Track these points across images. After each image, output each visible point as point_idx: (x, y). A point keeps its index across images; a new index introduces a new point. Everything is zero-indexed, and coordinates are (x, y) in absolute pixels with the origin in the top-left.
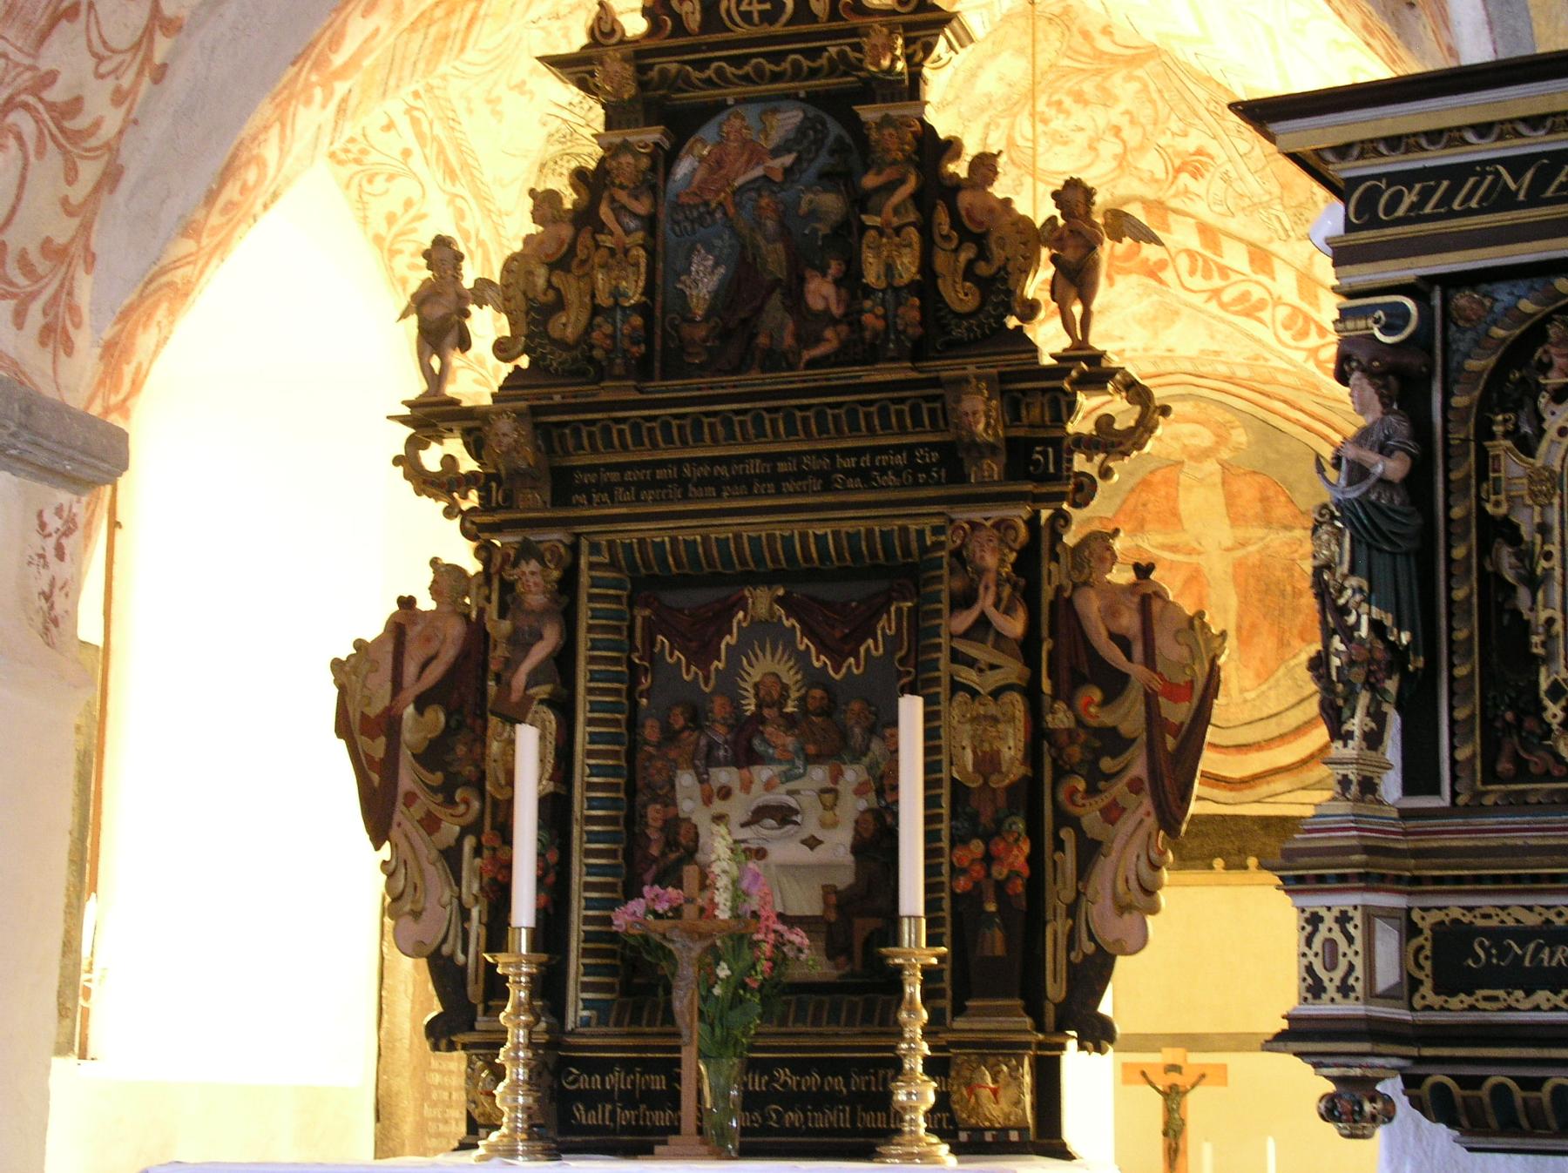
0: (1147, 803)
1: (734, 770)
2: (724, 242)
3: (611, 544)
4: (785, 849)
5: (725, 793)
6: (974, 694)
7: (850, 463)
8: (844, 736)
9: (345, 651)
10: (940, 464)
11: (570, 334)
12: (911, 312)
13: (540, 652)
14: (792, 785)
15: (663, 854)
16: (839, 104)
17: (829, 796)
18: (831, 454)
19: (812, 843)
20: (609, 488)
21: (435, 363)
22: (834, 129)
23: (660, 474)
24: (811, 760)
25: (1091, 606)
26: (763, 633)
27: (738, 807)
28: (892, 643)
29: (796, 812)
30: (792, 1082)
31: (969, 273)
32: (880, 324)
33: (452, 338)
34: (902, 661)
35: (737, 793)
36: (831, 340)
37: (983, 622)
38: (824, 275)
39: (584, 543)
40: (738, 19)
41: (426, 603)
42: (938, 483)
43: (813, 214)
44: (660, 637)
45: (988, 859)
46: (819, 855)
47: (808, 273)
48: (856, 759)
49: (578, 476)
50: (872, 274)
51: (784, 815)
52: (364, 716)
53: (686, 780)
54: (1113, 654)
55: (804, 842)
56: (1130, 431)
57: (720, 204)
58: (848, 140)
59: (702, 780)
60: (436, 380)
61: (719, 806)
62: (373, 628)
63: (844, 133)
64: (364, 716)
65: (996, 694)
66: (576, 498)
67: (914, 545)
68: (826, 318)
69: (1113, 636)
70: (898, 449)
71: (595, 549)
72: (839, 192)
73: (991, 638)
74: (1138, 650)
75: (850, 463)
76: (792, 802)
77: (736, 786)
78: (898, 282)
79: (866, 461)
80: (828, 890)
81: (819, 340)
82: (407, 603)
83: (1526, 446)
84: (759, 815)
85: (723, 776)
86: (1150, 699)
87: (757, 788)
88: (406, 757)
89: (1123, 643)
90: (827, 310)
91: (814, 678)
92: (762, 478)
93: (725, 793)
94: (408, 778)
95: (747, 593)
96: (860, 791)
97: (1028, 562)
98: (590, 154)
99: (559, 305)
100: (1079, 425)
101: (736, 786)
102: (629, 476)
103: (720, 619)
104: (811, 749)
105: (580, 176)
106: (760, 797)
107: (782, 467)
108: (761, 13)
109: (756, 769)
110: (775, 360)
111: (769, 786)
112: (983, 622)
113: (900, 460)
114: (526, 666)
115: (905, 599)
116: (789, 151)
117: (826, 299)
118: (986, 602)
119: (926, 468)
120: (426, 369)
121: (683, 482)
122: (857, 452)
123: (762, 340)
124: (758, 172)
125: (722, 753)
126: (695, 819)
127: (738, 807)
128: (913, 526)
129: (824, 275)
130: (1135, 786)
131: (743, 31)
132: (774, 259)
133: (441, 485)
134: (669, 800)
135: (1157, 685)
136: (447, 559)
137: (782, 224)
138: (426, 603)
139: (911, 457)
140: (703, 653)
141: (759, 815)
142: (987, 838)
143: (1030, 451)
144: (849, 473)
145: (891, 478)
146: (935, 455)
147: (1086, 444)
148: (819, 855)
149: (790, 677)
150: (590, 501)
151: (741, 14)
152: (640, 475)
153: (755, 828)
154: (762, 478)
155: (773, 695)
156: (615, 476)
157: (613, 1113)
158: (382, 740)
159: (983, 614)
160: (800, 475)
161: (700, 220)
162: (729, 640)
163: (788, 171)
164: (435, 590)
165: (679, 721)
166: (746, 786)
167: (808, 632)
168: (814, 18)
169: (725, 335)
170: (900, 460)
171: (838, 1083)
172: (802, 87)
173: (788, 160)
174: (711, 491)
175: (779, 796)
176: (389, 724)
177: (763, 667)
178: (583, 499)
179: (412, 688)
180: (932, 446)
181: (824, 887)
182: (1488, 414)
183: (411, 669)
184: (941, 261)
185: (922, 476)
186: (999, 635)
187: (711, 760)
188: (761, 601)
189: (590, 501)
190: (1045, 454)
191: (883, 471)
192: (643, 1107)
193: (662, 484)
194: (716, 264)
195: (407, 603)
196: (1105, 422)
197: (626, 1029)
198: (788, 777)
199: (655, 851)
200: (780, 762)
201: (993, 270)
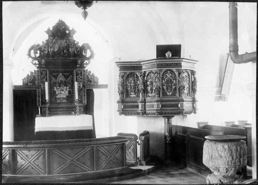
4: (63, 92)
9: (23, 78)
11: (46, 53)
17: (66, 89)
19: (65, 92)
24: (65, 86)
36: (66, 55)
37: (79, 77)
41: (30, 75)
51: (63, 90)
53: (55, 88)
54: (91, 80)
56: (88, 63)
59: (56, 88)
61: (58, 90)
62: (25, 77)
69: (91, 78)
79: (70, 64)
80: (66, 96)
82: (28, 75)
83: (128, 81)
93: (58, 89)
96: (68, 88)
98: (47, 39)
100: (85, 63)
101: (59, 88)
103: (57, 75)
106: (61, 89)
111: (62, 88)
112: (79, 77)
118: (79, 76)
127: (59, 90)
133: (35, 64)
134: (54, 89)
136: (32, 71)
138: (30, 75)
147: (85, 64)
148: (66, 93)
164: (31, 73)
175: (62, 89)
182: (35, 134)
195: (28, 75)
196: (86, 62)
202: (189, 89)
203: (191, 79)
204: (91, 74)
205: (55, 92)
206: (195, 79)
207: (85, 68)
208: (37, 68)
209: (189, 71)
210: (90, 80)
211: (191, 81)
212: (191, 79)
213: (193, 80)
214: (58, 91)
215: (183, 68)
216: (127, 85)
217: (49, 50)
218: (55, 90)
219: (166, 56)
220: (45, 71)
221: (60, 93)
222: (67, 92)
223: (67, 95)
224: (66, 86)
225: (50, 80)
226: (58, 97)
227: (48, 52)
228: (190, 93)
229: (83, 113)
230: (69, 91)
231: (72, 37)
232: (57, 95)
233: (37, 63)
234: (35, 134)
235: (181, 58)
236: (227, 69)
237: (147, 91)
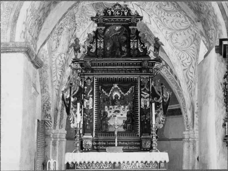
0: (162, 111)
1: (112, 106)
2: (111, 42)
3: (98, 78)
4: (118, 115)
5: (111, 109)
6: (144, 98)
7: (128, 70)
8: (126, 102)
10: (139, 70)
12: (136, 52)
13: (91, 91)
14: (120, 108)
15: (103, 116)
16: (127, 26)
18: (126, 68)
19: (122, 115)
20: (98, 71)
21: (76, 54)
22: (125, 29)
23: (105, 70)
24: (122, 105)
26: (116, 89)
27: (113, 111)
28: (132, 91)
29: (120, 111)
30: (121, 143)
31: (142, 48)
32: (133, 53)
33: (78, 51)
34: (133, 94)
35: (113, 109)
36: (125, 54)
38: (124, 46)
39: (95, 78)
40: (116, 15)
42: (139, 73)
43: (123, 39)
44: (103, 90)
45: (145, 117)
46: (123, 116)
47: (122, 46)
48: (127, 105)
49: (94, 69)
50: (132, 47)
51: (118, 112)
52: (66, 98)
53: (106, 107)
54: (158, 93)
55: (121, 115)
57: (111, 37)
58: (127, 31)
59: (108, 107)
60: (76, 56)
61: (110, 110)
63: (126, 29)
64: (66, 98)
65: (146, 98)
66: (94, 72)
67: (135, 79)
68: (124, 52)
70: (134, 68)
71: (96, 78)
72: (125, 37)
73: (146, 91)
74: (161, 94)
75: (128, 70)
76: (119, 110)
77: (112, 108)
78: (135, 48)
79: (130, 69)
80: (124, 121)
81: (124, 54)
84: (115, 111)
85: (111, 107)
86: (163, 99)
87: (115, 108)
88: (71, 103)
89: (160, 93)
90: (125, 51)
91: (122, 95)
92: (118, 71)
93: (111, 109)
95: (114, 85)
96: (127, 109)
99: (91, 48)
101: (112, 108)
102: (101, 70)
104: (122, 104)
105: (94, 32)
107: (120, 70)
108: (119, 14)
109: (115, 106)
110: (118, 56)
111: (117, 108)
112: (145, 89)
113: (134, 69)
114: (89, 93)
115: (133, 86)
116: (119, 31)
117: (124, 50)
118: (145, 87)
119: (137, 71)
120: (75, 55)
121: (107, 71)
122: (129, 68)
123: (116, 54)
124: (116, 33)
125: (110, 104)
126: (107, 112)
127: (113, 111)
128: (135, 78)
129: (124, 46)
130: (161, 109)
131: (116, 16)
132: (118, 45)
135: (164, 98)
137: (119, 40)
139: (136, 69)
140: (108, 92)
141: (115, 111)
142: (145, 115)
143: (149, 70)
144: (128, 71)
145: (133, 72)
146: (138, 69)
148: (123, 116)
149: (119, 95)
150: (96, 72)
151: (116, 14)
152: (102, 69)
153: (115, 113)
154: (118, 71)
155: (116, 97)
156: (99, 69)
157: (99, 147)
158: (68, 101)
159: (145, 88)
160: (122, 71)
161: (108, 39)
162: (112, 90)
163: (119, 34)
165: (105, 100)
166: (114, 108)
167: (121, 90)
168: (125, 15)
169: (112, 53)
170: (134, 69)
171: (126, 143)
172: (121, 24)
173: (120, 32)
174: (111, 72)
175: (118, 109)
176: (69, 99)
178: (95, 72)
179: (72, 95)
180: (138, 68)
181: (123, 120)
182: (168, 110)
183: (72, 92)
184: (139, 46)
185: (137, 72)
186: (147, 91)
187: (109, 105)
188: (116, 86)
189: (96, 72)
190: (151, 70)
191: (132, 71)
192: (103, 147)
193: (105, 71)
194: (110, 44)
197: (104, 137)
198: (119, 107)
199: (102, 115)
200: (118, 105)
201: (145, 47)
205: (105, 114)
210: (156, 94)
214: (110, 112)
218: (106, 110)
219: (148, 56)
220: (91, 80)
221: (114, 116)
222: (125, 115)
223: (126, 119)
224: (125, 104)
225: (99, 94)
226: (43, 158)
227: (97, 49)
229: (183, 116)
230: (129, 114)
232: (109, 119)
234: (168, 110)
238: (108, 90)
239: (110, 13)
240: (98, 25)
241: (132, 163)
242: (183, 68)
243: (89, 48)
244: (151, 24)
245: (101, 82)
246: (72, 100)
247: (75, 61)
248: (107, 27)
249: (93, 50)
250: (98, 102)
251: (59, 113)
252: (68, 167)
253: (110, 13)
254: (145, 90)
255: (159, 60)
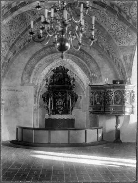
13: (51, 95)
22: (63, 74)
25: (73, 94)
50: (65, 80)
94: (45, 100)
97: (71, 93)
105: (53, 75)
176: (44, 97)
177: (60, 95)
202: (130, 101)
203: (131, 95)
204: (74, 93)
206: (134, 95)
207: (73, 89)
208: (48, 89)
209: (130, 91)
211: (131, 96)
212: (131, 95)
213: (133, 95)
215: (126, 89)
216: (95, 98)
217: (54, 80)
225: (54, 95)
227: (54, 81)
228: (130, 103)
231: (66, 73)
233: (48, 87)
235: (131, 84)
236: (92, 147)
237: (106, 101)
238: (57, 94)
239: (58, 69)
240: (54, 73)
241: (14, 43)
242: (86, 81)
243: (51, 81)
244: (73, 65)
245: (55, 92)
246: (45, 97)
247: (47, 85)
248: (57, 73)
249: (52, 81)
250: (54, 98)
251: (37, 98)
252: (97, 113)
253: (58, 69)
254: (69, 95)
255: (74, 85)
